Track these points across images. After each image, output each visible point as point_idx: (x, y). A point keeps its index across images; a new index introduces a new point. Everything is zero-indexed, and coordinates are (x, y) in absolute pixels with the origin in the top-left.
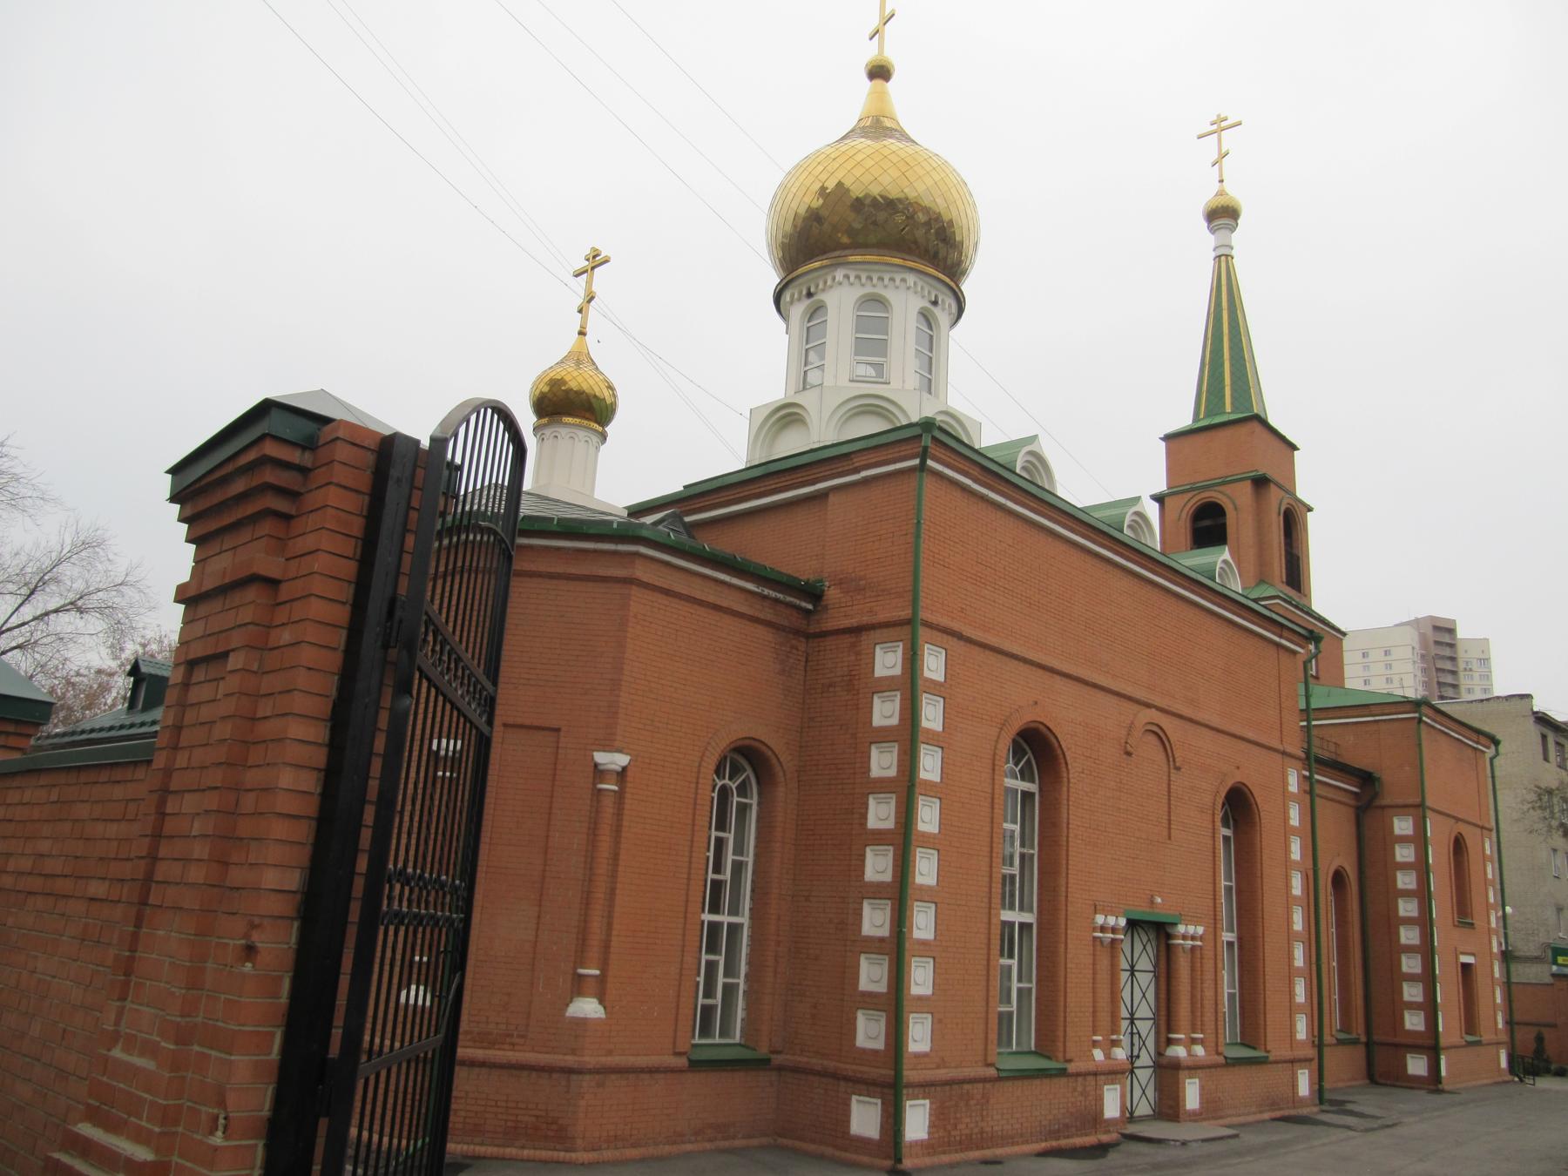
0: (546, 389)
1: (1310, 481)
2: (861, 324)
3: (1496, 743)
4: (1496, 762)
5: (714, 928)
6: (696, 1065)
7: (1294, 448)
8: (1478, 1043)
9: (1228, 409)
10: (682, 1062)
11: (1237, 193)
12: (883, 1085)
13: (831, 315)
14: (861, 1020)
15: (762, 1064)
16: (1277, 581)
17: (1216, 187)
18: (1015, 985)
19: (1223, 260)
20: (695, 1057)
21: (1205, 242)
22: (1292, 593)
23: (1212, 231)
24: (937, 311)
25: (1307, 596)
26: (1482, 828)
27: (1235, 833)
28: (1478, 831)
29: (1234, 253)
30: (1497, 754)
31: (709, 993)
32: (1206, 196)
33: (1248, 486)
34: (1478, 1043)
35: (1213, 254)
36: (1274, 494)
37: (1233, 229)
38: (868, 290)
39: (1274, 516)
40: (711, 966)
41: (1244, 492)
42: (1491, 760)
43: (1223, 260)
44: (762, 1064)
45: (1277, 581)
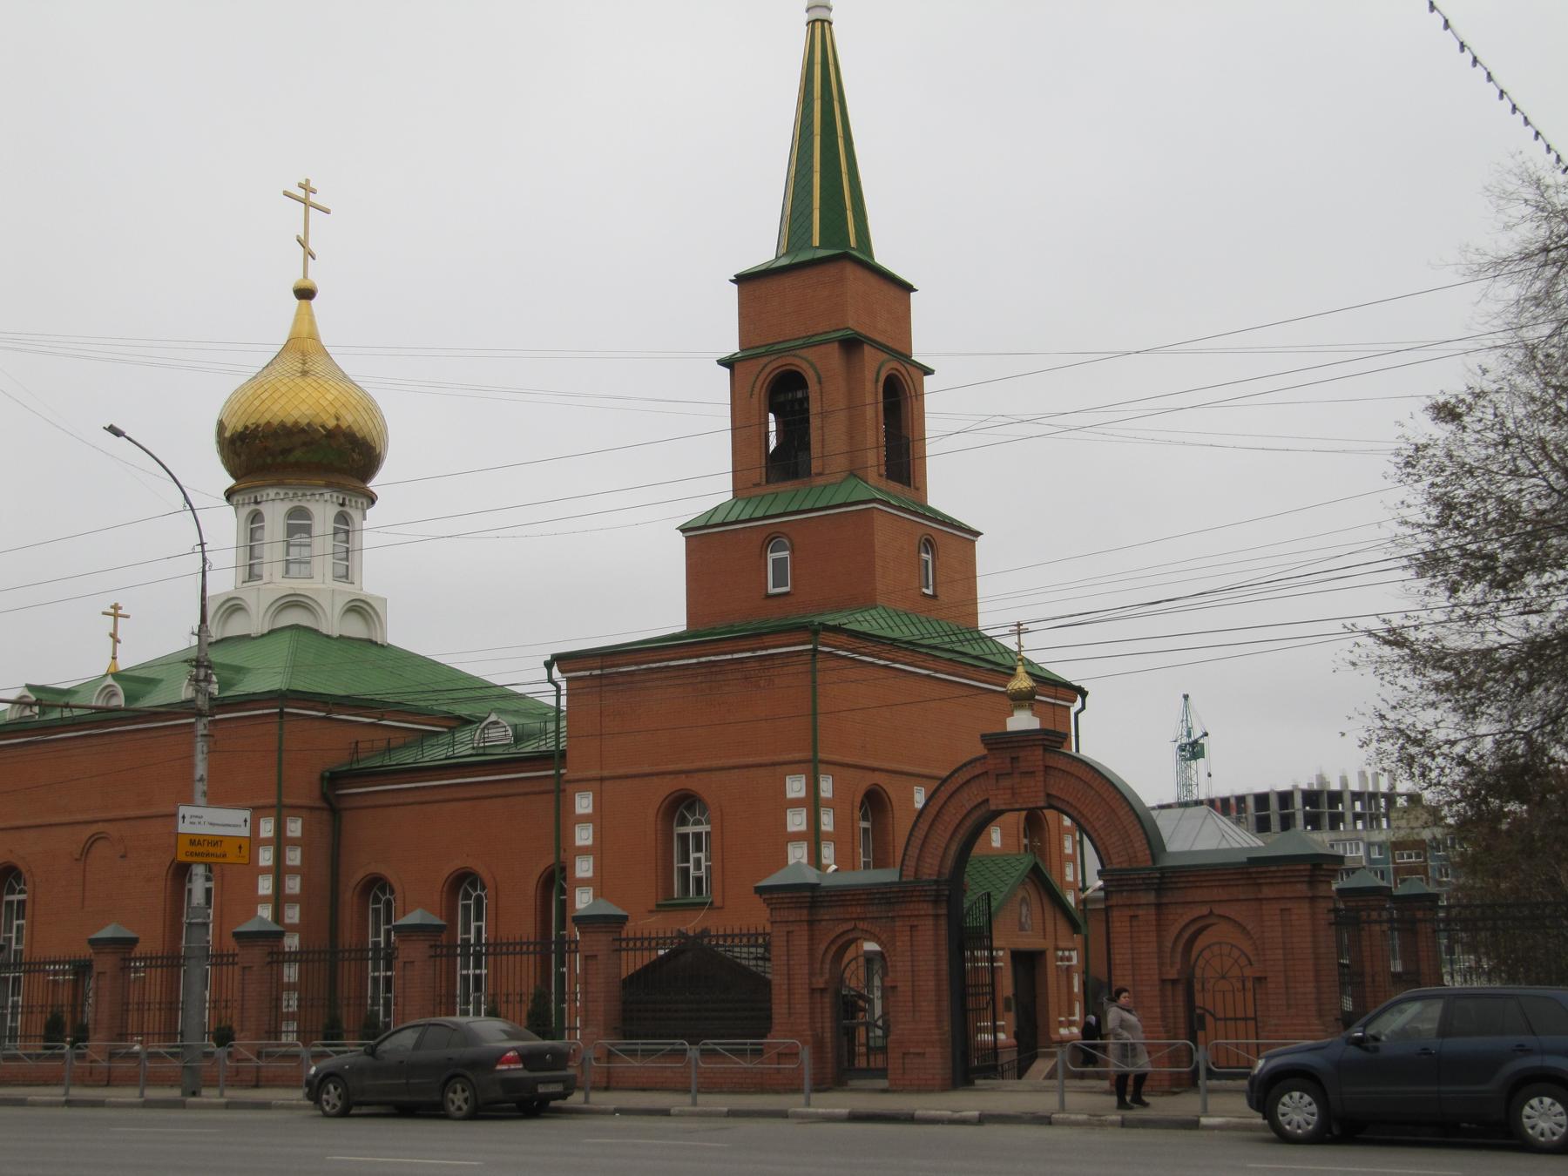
1: (926, 341)
2: (291, 531)
3: (1084, 694)
5: (388, 967)
7: (908, 288)
9: (816, 242)
12: (273, 807)
13: (267, 523)
14: (297, 862)
16: (872, 475)
18: (14, 935)
22: (896, 487)
24: (346, 509)
25: (921, 490)
29: (833, 16)
30: (1083, 707)
31: (479, 929)
35: (805, 17)
38: (296, 503)
39: (869, 386)
40: (18, 941)
41: (833, 358)
42: (1076, 715)
45: (872, 475)
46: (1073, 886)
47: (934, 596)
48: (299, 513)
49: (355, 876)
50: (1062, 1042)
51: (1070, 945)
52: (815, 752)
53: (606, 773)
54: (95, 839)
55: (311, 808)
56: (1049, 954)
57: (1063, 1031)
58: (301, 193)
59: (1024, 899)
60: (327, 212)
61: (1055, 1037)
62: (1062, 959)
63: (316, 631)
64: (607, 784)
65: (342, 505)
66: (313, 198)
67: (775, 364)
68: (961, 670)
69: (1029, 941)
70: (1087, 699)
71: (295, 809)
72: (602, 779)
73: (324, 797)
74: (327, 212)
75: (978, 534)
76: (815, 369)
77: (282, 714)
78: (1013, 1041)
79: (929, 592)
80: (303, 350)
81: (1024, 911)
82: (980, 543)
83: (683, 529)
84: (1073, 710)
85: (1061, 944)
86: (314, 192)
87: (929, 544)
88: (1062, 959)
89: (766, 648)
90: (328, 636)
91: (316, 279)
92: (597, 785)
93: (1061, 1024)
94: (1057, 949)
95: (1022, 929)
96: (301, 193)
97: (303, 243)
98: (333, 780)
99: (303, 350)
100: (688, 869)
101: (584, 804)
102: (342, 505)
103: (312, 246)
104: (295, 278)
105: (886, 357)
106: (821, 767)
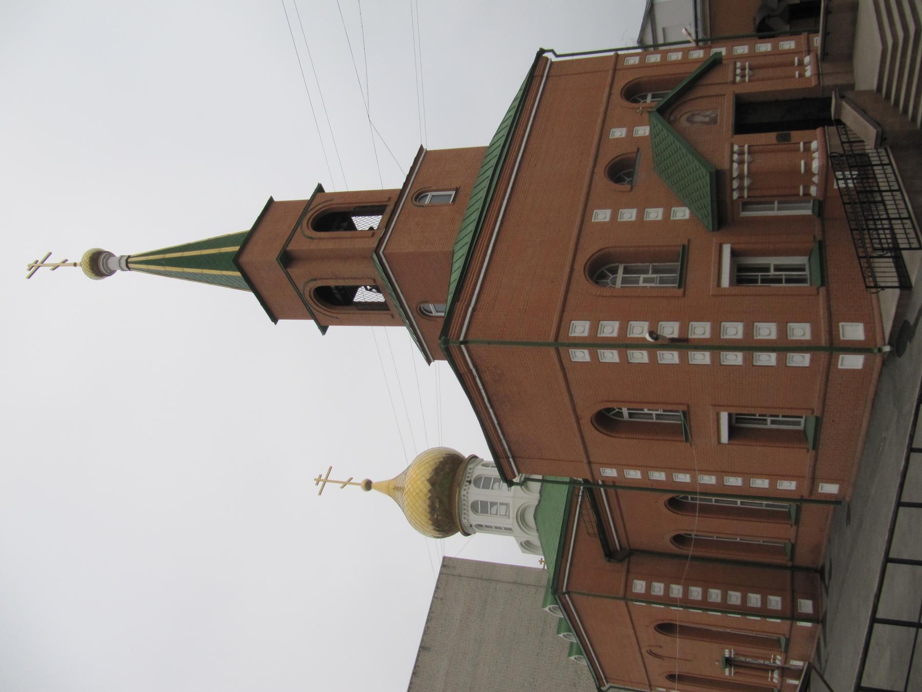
0: (430, 495)
3: (542, 52)
4: (558, 53)
6: (824, 282)
7: (271, 201)
8: (788, 641)
10: (823, 290)
11: (79, 254)
15: (821, 245)
17: (79, 268)
19: (129, 263)
20: (819, 282)
21: (121, 277)
23: (111, 273)
24: (473, 479)
26: (615, 70)
27: (621, 263)
28: (619, 74)
30: (552, 51)
32: (80, 276)
33: (295, 271)
34: (788, 641)
36: (299, 245)
37: (110, 255)
42: (557, 56)
43: (129, 263)
44: (821, 245)
46: (686, 52)
47: (457, 190)
48: (474, 507)
49: (674, 549)
50: (818, 75)
51: (731, 67)
52: (549, 345)
53: (585, 461)
54: (651, 653)
55: (628, 572)
56: (739, 90)
57: (808, 74)
58: (321, 483)
59: (689, 120)
60: (331, 468)
61: (814, 83)
62: (743, 76)
63: (537, 506)
64: (592, 459)
65: (470, 482)
66: (323, 477)
67: (314, 305)
68: (507, 171)
69: (726, 114)
70: (546, 48)
71: (628, 585)
72: (589, 463)
73: (621, 561)
74: (331, 468)
75: (421, 148)
76: (309, 282)
77: (568, 592)
78: (819, 131)
79: (453, 193)
80: (394, 489)
81: (698, 119)
82: (429, 147)
83: (429, 362)
84: (554, 59)
85: (730, 79)
86: (321, 476)
87: (419, 196)
88: (743, 76)
89: (470, 371)
90: (539, 502)
91: (361, 479)
92: (593, 466)
93: (801, 75)
94: (734, 82)
95: (714, 121)
96: (321, 483)
97: (345, 484)
98: (610, 554)
99: (394, 489)
100: (657, 415)
101: (610, 473)
102: (470, 482)
103: (346, 480)
104: (360, 490)
105: (299, 230)
106: (562, 339)
